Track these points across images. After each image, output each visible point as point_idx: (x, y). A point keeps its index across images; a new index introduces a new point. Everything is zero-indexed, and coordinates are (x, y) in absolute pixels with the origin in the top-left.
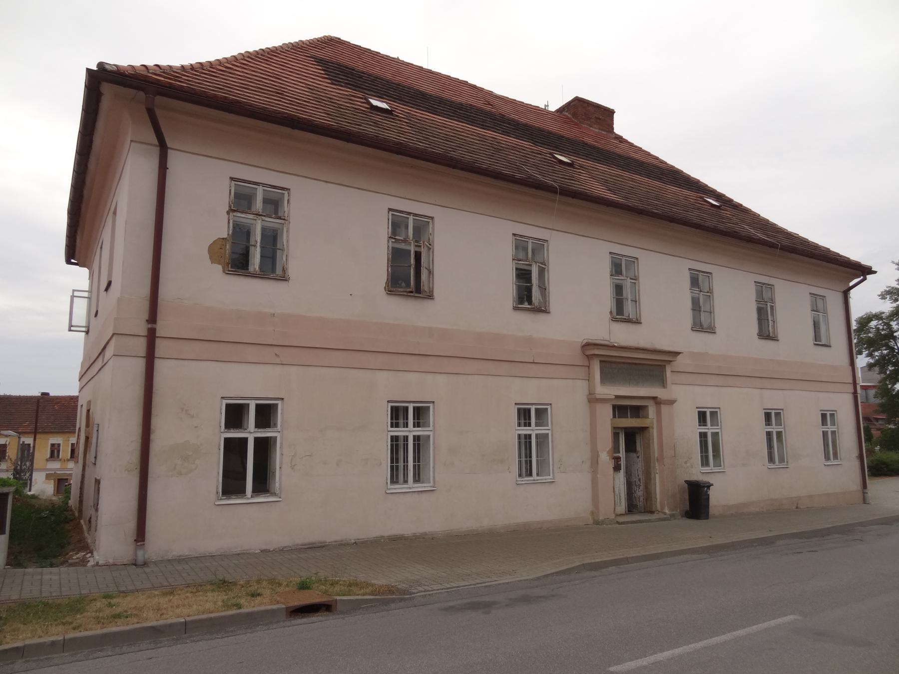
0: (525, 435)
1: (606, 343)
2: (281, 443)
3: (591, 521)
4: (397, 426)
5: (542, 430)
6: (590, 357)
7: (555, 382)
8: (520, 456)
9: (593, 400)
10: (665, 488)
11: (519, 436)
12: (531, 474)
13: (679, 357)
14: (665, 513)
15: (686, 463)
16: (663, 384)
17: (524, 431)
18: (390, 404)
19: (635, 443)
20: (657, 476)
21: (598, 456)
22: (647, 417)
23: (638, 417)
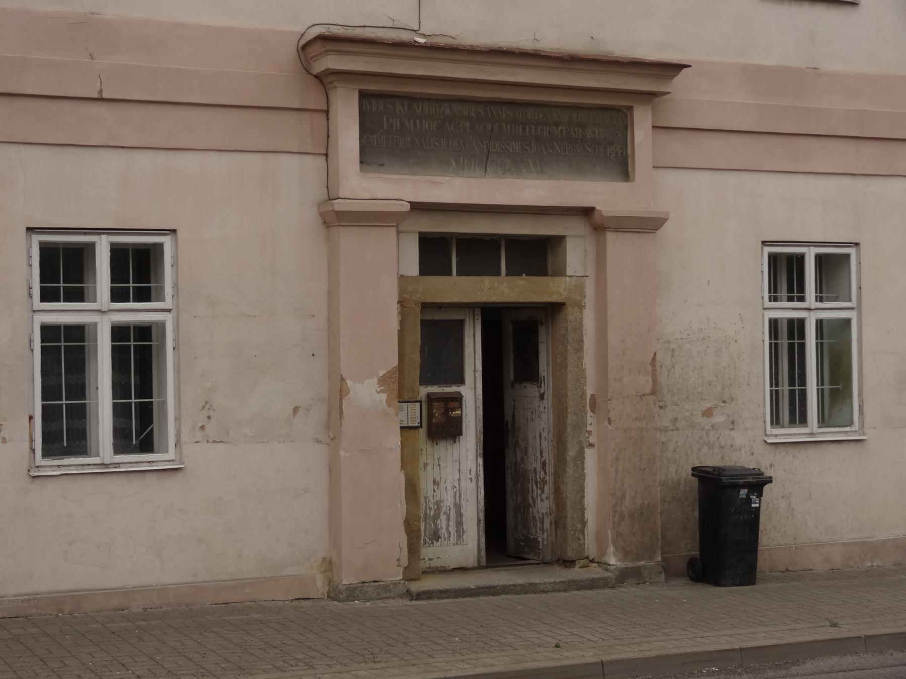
0: (791, 321)
1: (405, 36)
2: (176, 340)
3: (320, 587)
4: (776, 299)
5: (832, 312)
6: (325, 81)
7: (190, 162)
8: (775, 380)
9: (336, 219)
10: (601, 485)
11: (774, 324)
12: (803, 421)
13: (679, 84)
14: (604, 565)
15: (708, 413)
16: (623, 168)
17: (786, 311)
18: (768, 250)
19: (536, 353)
20: (590, 456)
21: (343, 392)
22: (560, 272)
23: (542, 271)
